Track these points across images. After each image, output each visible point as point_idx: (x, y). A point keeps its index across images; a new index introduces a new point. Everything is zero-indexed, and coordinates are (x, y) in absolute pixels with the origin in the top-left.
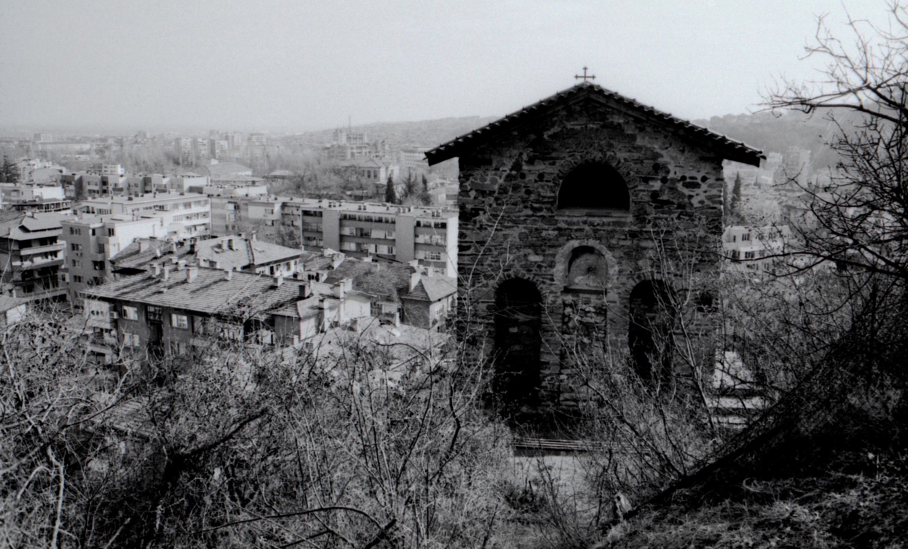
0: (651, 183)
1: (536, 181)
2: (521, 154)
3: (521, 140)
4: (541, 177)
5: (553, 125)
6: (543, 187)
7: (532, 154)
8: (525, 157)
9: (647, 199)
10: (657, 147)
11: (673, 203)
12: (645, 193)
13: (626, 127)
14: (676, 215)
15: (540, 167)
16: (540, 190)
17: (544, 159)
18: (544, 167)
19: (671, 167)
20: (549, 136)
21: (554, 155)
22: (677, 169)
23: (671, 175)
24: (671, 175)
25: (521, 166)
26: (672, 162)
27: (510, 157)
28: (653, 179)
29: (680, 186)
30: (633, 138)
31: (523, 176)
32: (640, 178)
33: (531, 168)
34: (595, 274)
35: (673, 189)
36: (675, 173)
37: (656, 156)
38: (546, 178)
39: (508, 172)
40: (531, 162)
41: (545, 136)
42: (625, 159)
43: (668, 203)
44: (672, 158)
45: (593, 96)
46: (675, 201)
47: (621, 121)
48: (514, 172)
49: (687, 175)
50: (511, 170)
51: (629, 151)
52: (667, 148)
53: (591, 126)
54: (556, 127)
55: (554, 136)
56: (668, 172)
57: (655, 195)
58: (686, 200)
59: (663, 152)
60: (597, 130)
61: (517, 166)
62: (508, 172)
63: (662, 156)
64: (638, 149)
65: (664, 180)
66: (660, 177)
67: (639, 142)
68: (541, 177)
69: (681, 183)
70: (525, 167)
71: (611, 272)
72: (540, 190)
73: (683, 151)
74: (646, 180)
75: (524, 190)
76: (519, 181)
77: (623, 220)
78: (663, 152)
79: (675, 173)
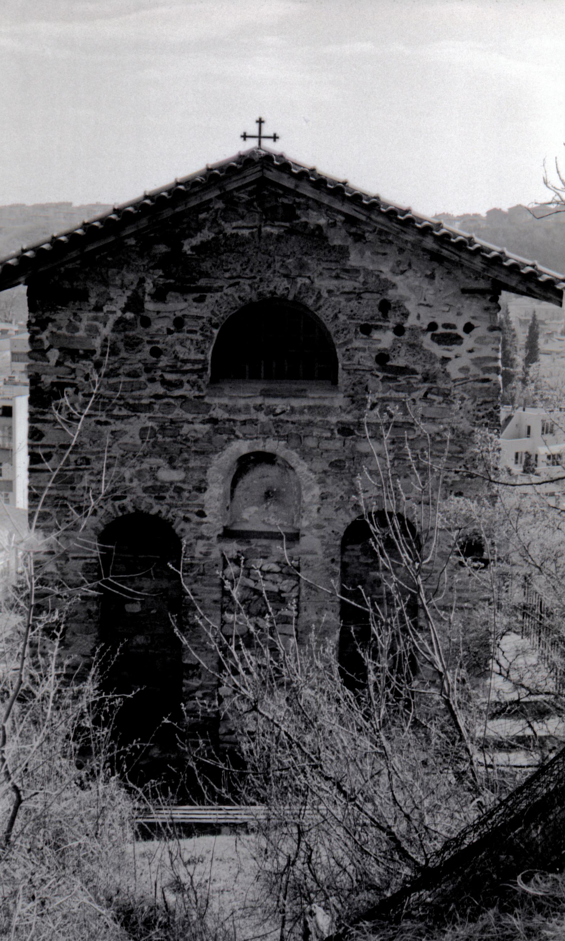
0: (376, 335)
1: (170, 332)
2: (142, 281)
3: (141, 255)
4: (179, 323)
5: (199, 228)
6: (182, 343)
7: (161, 281)
8: (149, 287)
9: (370, 363)
10: (386, 270)
11: (414, 372)
12: (366, 354)
13: (330, 233)
14: (422, 393)
15: (177, 305)
16: (178, 348)
17: (183, 289)
18: (183, 305)
19: (410, 306)
20: (193, 248)
22: (423, 311)
23: (411, 322)
24: (411, 322)
26: (413, 297)
28: (378, 328)
30: (343, 252)
31: (146, 322)
33: (160, 306)
34: (278, 502)
36: (419, 317)
37: (387, 285)
38: (189, 324)
39: (119, 314)
40: (159, 296)
41: (186, 248)
42: (330, 292)
44: (412, 289)
45: (272, 175)
46: (419, 368)
47: (322, 221)
48: (129, 315)
50: (124, 311)
51: (337, 277)
52: (403, 272)
53: (268, 229)
54: (205, 231)
55: (202, 249)
56: (406, 315)
57: (382, 358)
58: (438, 365)
59: (397, 279)
60: (279, 238)
61: (135, 303)
62: (119, 314)
63: (394, 286)
64: (354, 272)
65: (399, 330)
66: (391, 325)
68: (179, 323)
69: (429, 334)
70: (150, 306)
71: (307, 498)
72: (178, 348)
73: (432, 277)
74: (366, 330)
75: (148, 348)
76: (138, 331)
77: (327, 403)
78: (397, 279)
79: (419, 317)
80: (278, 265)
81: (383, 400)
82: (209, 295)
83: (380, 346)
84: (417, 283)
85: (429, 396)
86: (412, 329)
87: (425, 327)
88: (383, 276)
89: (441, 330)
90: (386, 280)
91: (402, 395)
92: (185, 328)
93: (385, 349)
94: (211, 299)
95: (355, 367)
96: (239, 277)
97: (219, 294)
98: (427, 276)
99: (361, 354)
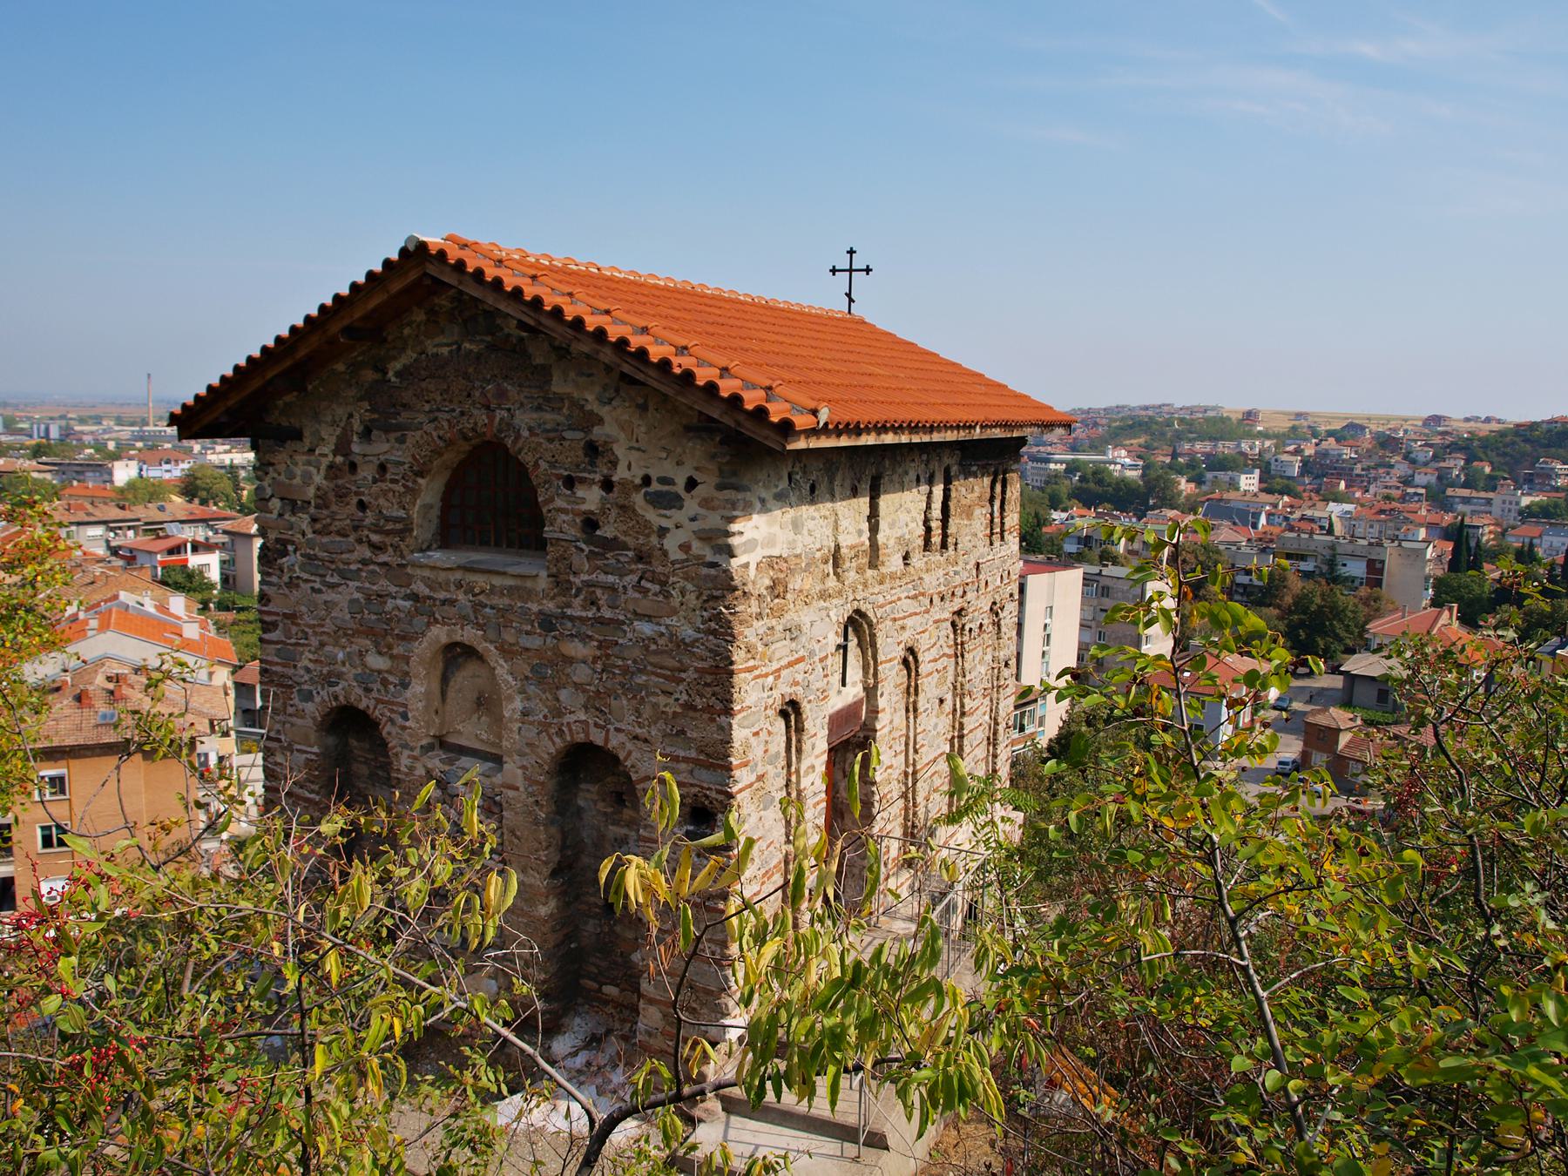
7: (368, 416)
8: (357, 425)
9: (573, 532)
16: (381, 501)
18: (386, 447)
19: (619, 451)
21: (404, 417)
22: (635, 455)
23: (620, 474)
24: (620, 474)
25: (350, 442)
27: (334, 423)
28: (583, 481)
29: (638, 499)
30: (544, 373)
31: (353, 467)
32: (558, 477)
33: (368, 449)
35: (626, 509)
38: (391, 469)
43: (612, 544)
46: (629, 541)
49: (654, 474)
51: (539, 408)
54: (409, 352)
56: (614, 464)
57: (590, 524)
58: (654, 540)
59: (604, 411)
60: (479, 357)
61: (342, 447)
62: (331, 457)
63: (601, 421)
65: (607, 485)
67: (558, 386)
70: (356, 448)
75: (355, 500)
78: (604, 411)
80: (477, 394)
81: (588, 584)
82: (410, 434)
83: (584, 507)
84: (626, 417)
85: (643, 583)
86: (624, 483)
87: (638, 481)
88: (588, 407)
89: (655, 486)
90: (591, 413)
91: (611, 579)
92: (388, 476)
93: (592, 512)
94: (413, 437)
95: (556, 535)
96: (439, 410)
97: (419, 433)
98: (638, 406)
99: (565, 518)
